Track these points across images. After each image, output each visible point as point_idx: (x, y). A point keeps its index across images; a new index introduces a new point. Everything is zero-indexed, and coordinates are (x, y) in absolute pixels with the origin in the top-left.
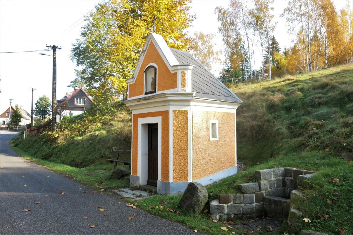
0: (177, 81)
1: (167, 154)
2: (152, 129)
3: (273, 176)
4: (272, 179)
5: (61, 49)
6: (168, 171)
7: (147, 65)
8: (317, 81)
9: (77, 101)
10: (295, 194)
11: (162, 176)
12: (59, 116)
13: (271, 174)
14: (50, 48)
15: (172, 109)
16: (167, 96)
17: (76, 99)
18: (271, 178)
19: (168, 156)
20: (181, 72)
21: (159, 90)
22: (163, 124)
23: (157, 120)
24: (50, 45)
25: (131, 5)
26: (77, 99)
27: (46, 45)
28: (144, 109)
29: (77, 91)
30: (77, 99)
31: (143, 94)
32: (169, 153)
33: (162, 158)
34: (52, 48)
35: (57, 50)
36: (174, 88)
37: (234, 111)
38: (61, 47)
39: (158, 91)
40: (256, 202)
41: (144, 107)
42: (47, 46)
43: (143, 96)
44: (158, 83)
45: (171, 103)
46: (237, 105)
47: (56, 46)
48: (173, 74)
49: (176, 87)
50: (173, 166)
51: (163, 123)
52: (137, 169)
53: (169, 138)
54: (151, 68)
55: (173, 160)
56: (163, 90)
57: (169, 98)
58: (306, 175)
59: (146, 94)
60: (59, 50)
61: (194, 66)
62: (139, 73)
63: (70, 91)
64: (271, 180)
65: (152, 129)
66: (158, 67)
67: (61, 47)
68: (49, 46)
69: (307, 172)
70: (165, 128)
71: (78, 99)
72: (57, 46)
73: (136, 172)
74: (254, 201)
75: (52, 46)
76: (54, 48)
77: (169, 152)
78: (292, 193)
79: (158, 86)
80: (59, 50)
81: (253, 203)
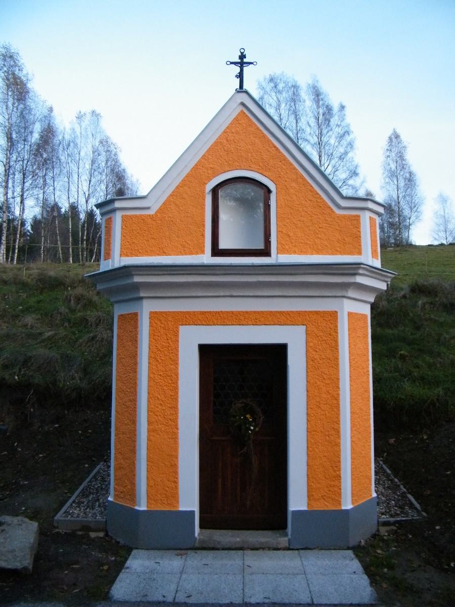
43: (206, 258)
45: (351, 293)
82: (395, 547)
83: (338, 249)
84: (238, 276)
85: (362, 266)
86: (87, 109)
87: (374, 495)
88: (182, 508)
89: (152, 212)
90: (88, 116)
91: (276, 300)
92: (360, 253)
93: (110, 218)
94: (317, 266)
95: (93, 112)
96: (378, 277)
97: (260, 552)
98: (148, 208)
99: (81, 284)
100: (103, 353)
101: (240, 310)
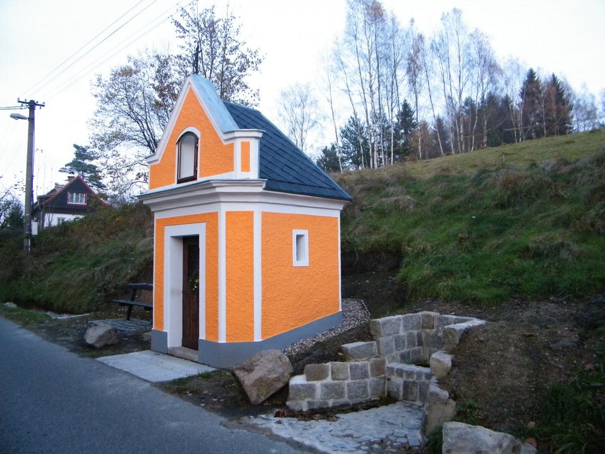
0: (233, 158)
1: (215, 292)
2: (190, 245)
3: (401, 328)
4: (400, 334)
5: (44, 106)
6: (217, 321)
7: (183, 130)
8: (93, 264)
9: (72, 198)
10: (438, 361)
11: (206, 331)
12: (36, 223)
13: (399, 326)
14: (24, 105)
15: (224, 209)
16: (214, 185)
17: (76, 194)
18: (398, 330)
19: (218, 295)
20: (243, 143)
21: (201, 176)
22: (207, 237)
23: (198, 229)
24: (26, 100)
25: (234, 98)
26: (72, 193)
27: (19, 99)
28: (198, 207)
29: (73, 180)
30: (72, 193)
31: (174, 182)
32: (218, 289)
33: (207, 299)
34: (28, 104)
35: (37, 108)
36: (228, 171)
37: (337, 215)
38: (44, 103)
39: (200, 177)
40: (373, 375)
41: (175, 206)
42: (19, 102)
43: (175, 185)
44: (200, 163)
45: (222, 199)
46: (341, 203)
47: (35, 102)
48: (226, 146)
49: (233, 170)
50: (227, 314)
51: (263, 219)
52: (162, 319)
53: (219, 262)
54: (190, 135)
55: (227, 302)
56: (209, 175)
57: (218, 190)
58: (457, 324)
59: (179, 182)
60: (40, 108)
61: (265, 131)
62: (168, 144)
63: (63, 180)
64: (397, 335)
65: (190, 245)
66: (201, 137)
67: (44, 103)
68: (24, 101)
69: (458, 319)
70: (212, 244)
71: (75, 194)
72: (37, 102)
73: (161, 324)
74: (370, 373)
75: (28, 101)
76: (32, 105)
77: (219, 288)
78: (433, 359)
79: (201, 167)
80: (40, 108)
81: (368, 377)
82: (567, 309)
83: (224, 169)
84: (178, 195)
85: (211, 182)
86: (449, 9)
87: (341, 310)
88: (164, 331)
89: (158, 162)
90: (451, 14)
91: (196, 207)
92: (200, 177)
93: (233, 144)
94: (180, 189)
95: (454, 9)
96: (234, 185)
97: (187, 361)
98: (157, 160)
99: (64, 229)
100: (452, 171)
101: (205, 212)
